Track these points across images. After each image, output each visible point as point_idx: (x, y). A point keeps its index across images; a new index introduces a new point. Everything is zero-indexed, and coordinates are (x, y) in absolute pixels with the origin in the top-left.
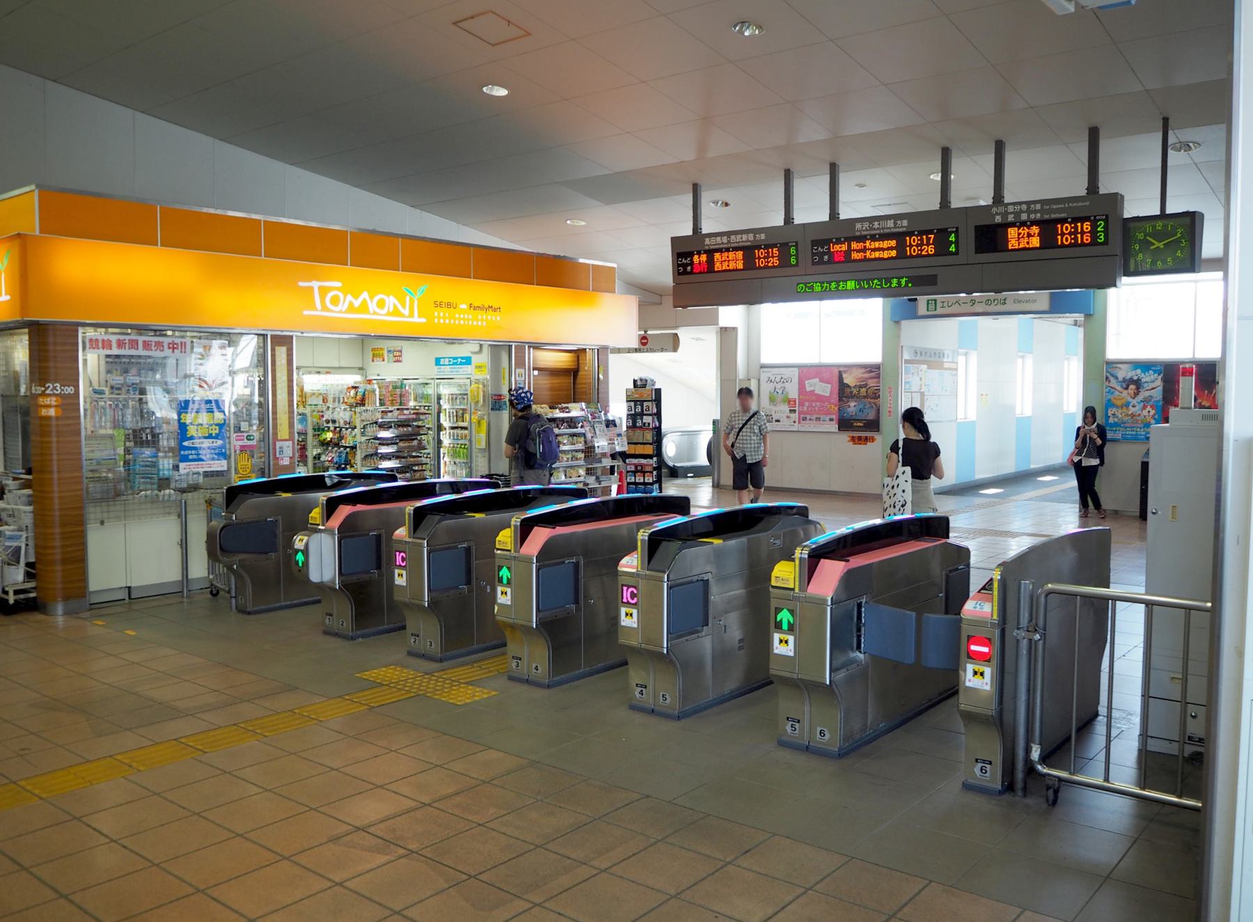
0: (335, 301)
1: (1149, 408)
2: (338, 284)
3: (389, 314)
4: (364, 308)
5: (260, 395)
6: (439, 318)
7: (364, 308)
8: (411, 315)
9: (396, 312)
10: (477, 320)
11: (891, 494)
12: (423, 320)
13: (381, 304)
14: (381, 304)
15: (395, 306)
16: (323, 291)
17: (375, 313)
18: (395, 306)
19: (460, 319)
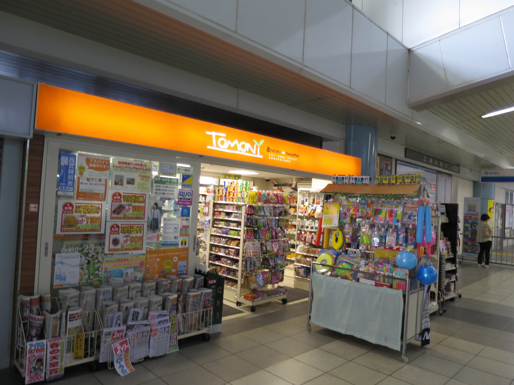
0: (222, 143)
1: (334, 211)
2: (224, 135)
3: (246, 152)
4: (235, 148)
5: (34, 217)
6: (271, 156)
7: (235, 148)
8: (256, 153)
9: (250, 151)
10: (282, 158)
11: (133, 293)
12: (261, 157)
13: (243, 146)
14: (243, 146)
15: (249, 149)
16: (217, 137)
17: (240, 151)
18: (249, 149)
19: (279, 158)
